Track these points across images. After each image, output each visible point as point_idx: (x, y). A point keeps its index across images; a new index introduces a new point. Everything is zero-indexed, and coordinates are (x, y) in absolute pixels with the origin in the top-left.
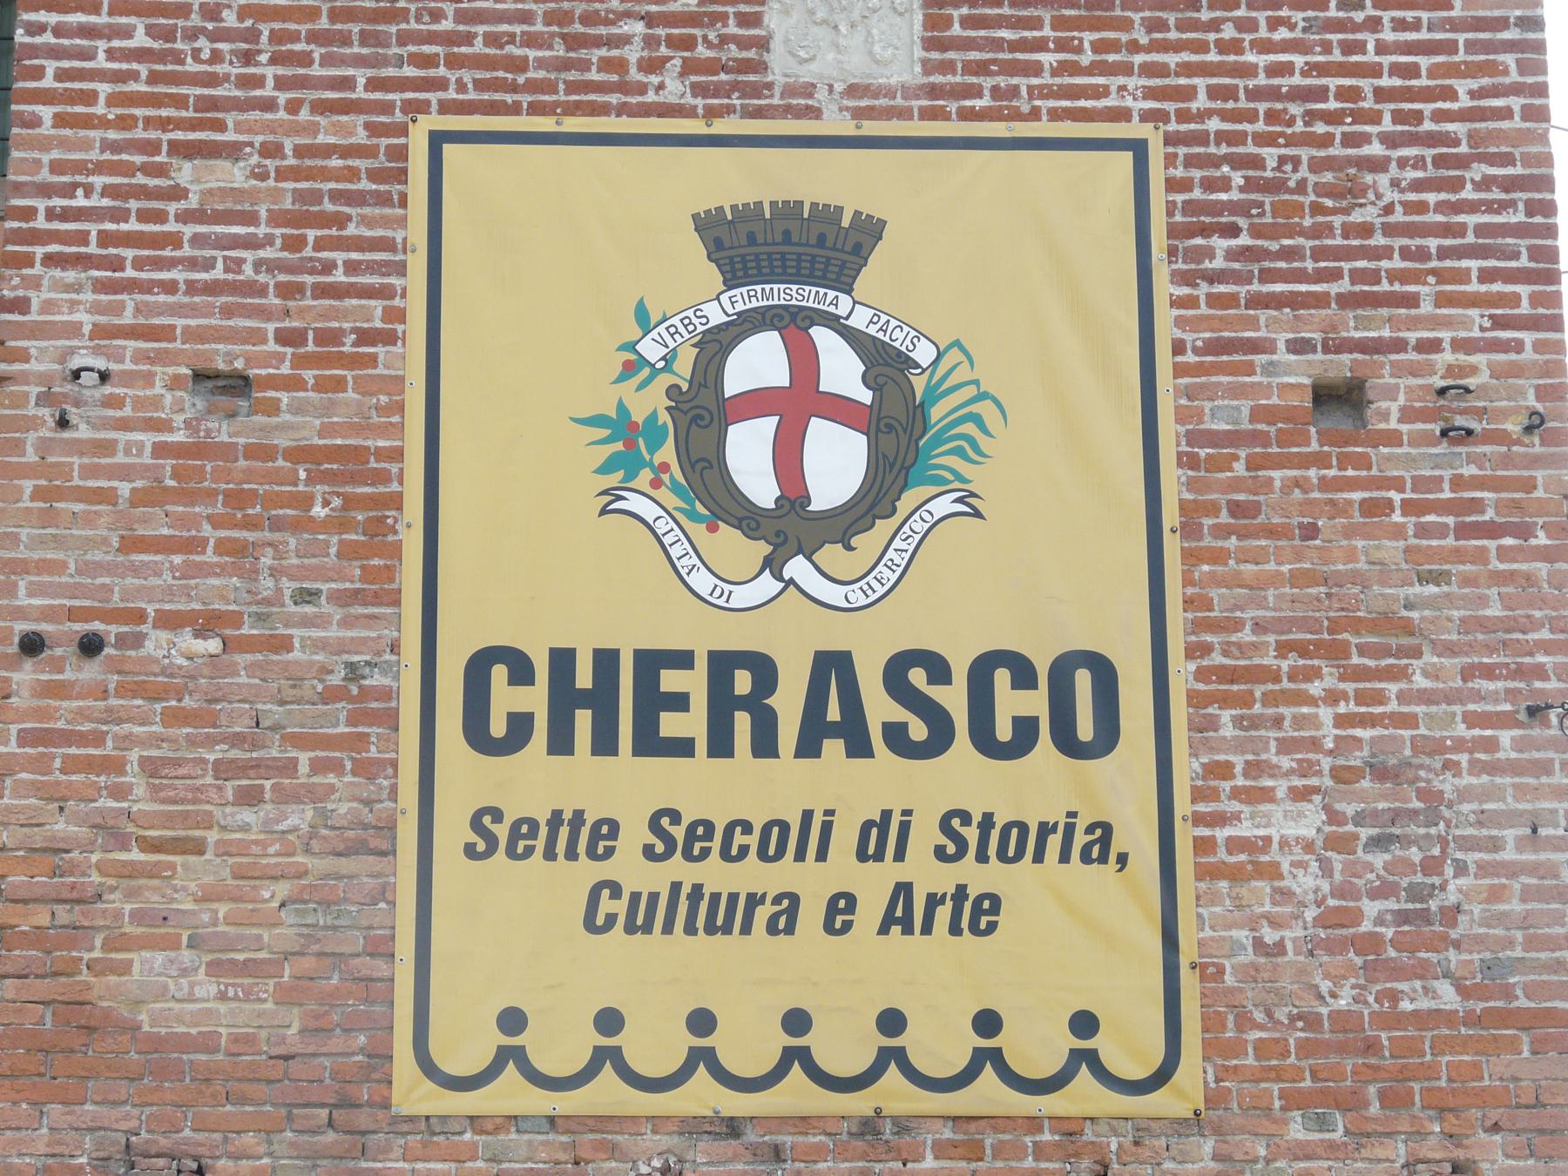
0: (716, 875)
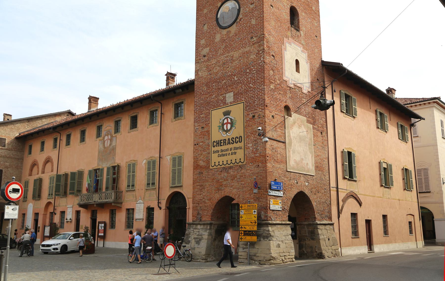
0: (224, 153)
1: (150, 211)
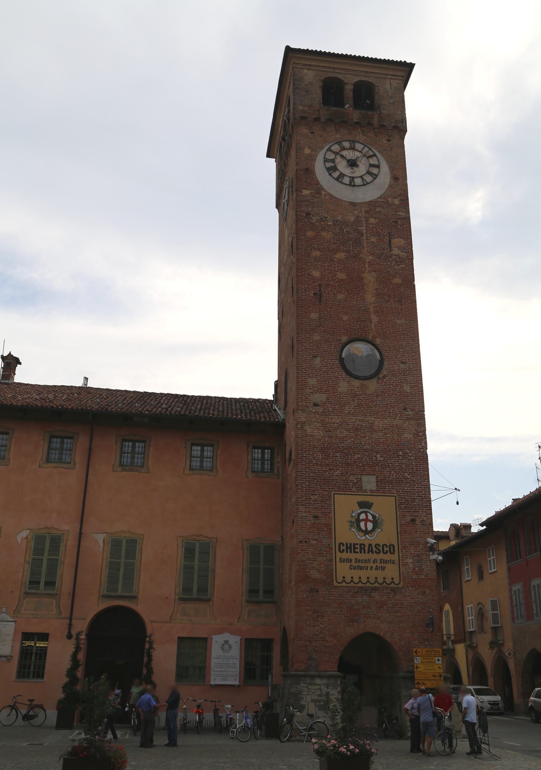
0: (361, 564)
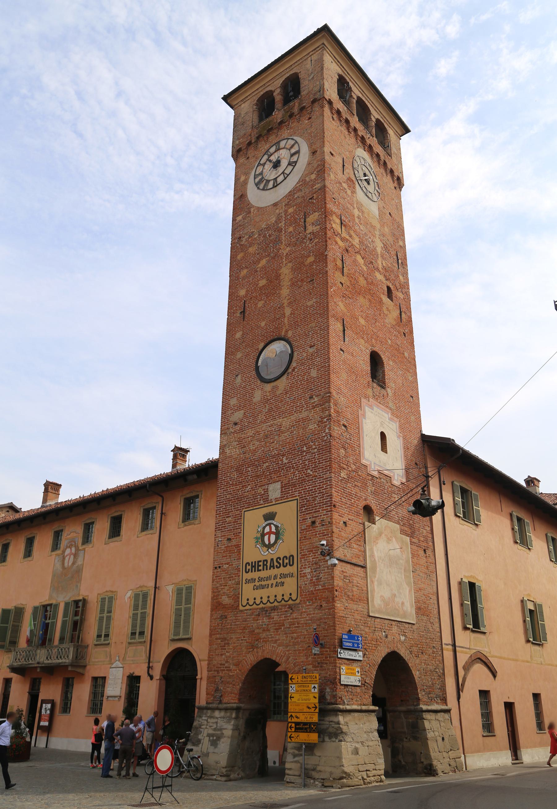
0: (263, 583)
1: (133, 682)
